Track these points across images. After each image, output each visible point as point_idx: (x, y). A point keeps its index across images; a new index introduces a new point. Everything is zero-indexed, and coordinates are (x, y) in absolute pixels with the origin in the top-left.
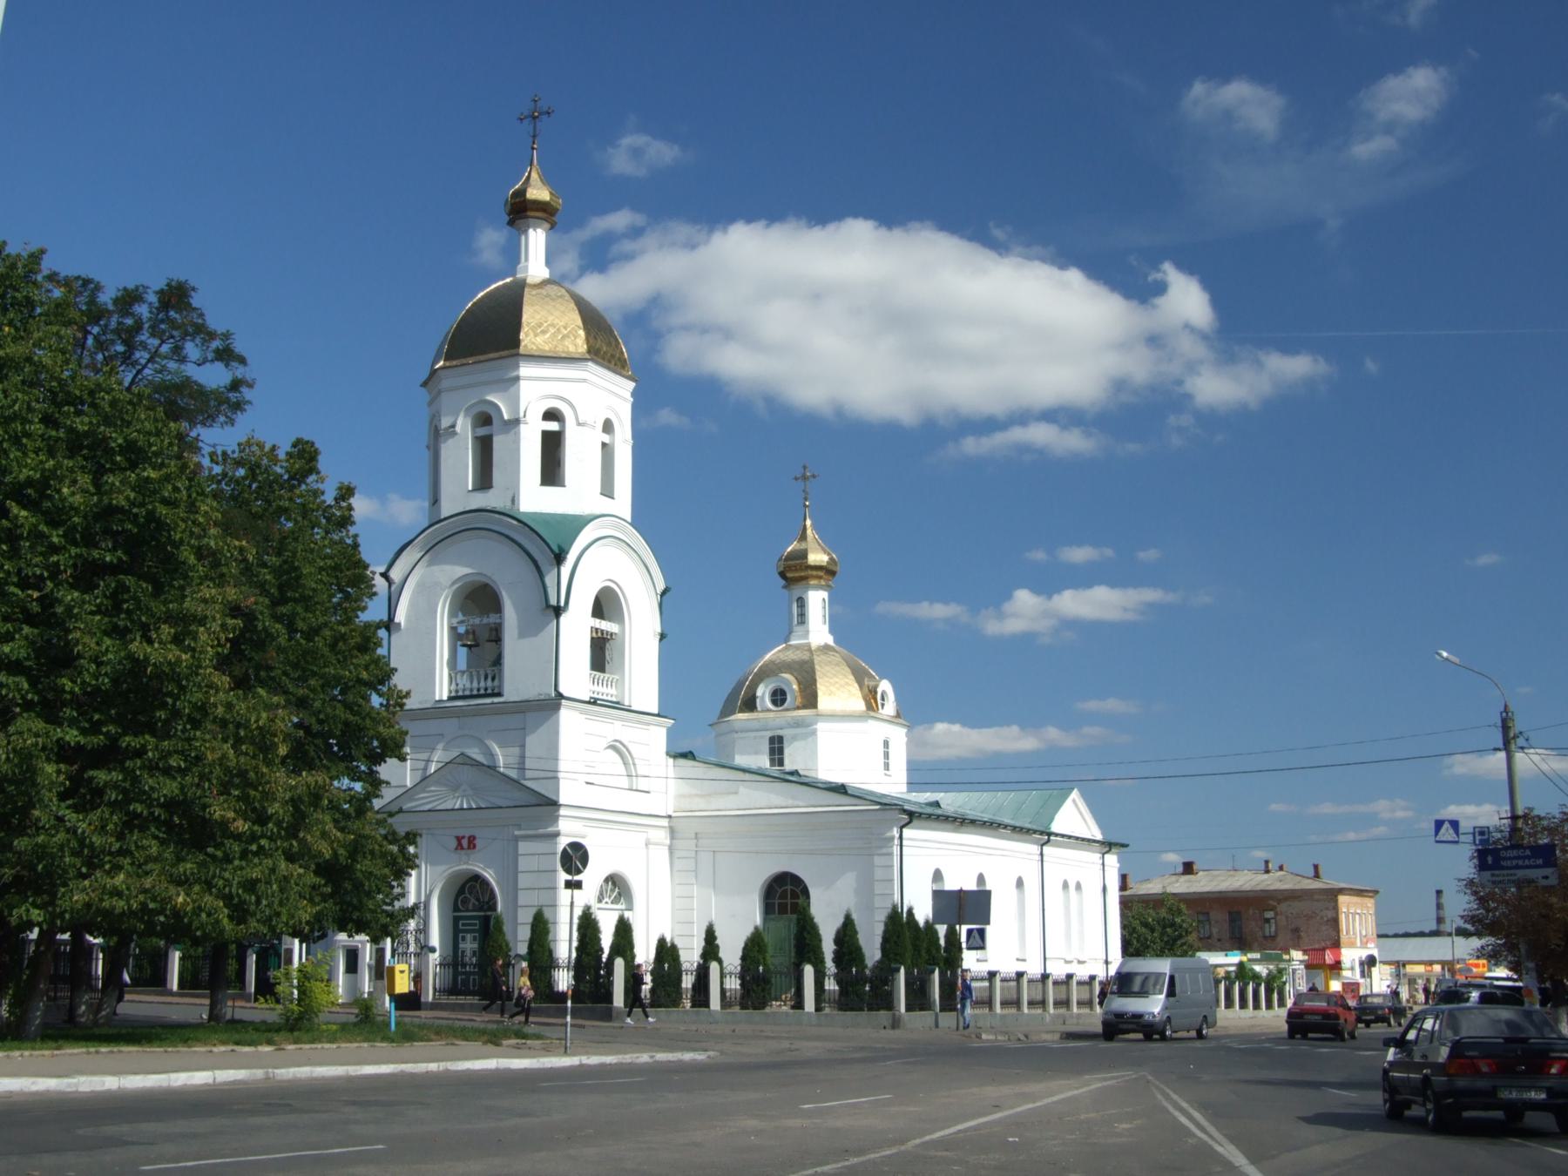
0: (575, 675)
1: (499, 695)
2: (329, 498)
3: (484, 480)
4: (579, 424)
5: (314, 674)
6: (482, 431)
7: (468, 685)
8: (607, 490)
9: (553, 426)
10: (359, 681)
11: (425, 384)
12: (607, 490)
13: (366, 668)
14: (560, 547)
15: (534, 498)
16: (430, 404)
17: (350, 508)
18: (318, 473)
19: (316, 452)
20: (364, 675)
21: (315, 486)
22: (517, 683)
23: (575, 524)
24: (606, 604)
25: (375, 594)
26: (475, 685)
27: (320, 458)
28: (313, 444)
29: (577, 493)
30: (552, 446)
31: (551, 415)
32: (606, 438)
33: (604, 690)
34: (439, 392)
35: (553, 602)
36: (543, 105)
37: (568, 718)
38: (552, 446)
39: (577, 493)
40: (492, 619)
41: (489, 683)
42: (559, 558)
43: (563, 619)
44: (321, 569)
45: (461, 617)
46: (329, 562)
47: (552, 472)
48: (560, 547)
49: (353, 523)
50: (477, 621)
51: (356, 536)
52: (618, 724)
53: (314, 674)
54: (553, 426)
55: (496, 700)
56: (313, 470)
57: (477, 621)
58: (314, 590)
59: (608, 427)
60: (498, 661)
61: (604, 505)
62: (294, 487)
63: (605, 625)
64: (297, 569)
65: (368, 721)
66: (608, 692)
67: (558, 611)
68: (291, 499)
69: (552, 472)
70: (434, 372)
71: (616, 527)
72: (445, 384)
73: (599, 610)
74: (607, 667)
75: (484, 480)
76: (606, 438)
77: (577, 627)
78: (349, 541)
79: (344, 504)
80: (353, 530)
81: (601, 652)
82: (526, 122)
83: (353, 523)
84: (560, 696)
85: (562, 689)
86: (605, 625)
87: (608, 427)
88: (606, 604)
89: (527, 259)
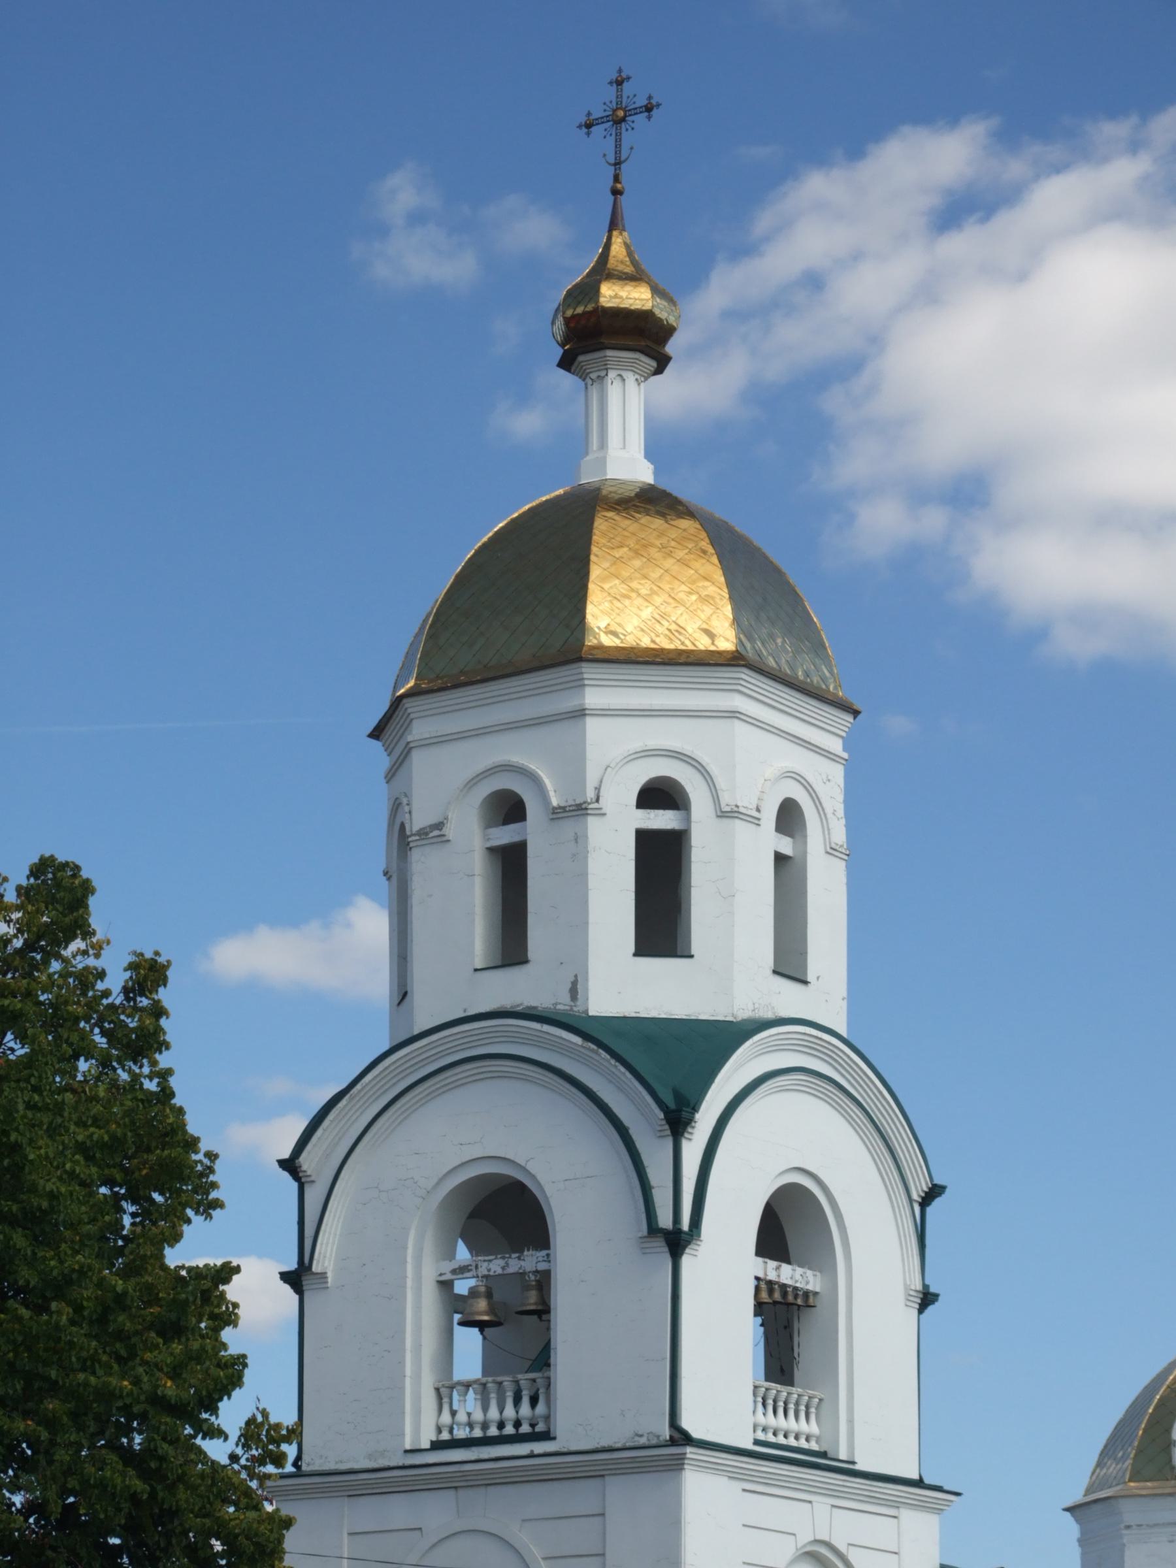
0: (721, 1385)
1: (546, 1436)
2: (115, 981)
3: (511, 946)
4: (722, 815)
5: (53, 1388)
6: (505, 835)
7: (478, 1416)
8: (790, 964)
9: (662, 820)
10: (158, 1401)
11: (377, 733)
12: (790, 964)
13: (175, 1373)
14: (678, 1096)
15: (625, 985)
16: (390, 776)
17: (158, 1011)
18: (87, 933)
19: (87, 888)
20: (169, 1387)
21: (80, 963)
22: (589, 1402)
23: (716, 1041)
24: (787, 1224)
25: (217, 1204)
26: (493, 1413)
27: (92, 901)
28: (77, 868)
29: (724, 970)
30: (662, 868)
31: (658, 794)
32: (786, 846)
33: (791, 1424)
34: (408, 751)
35: (665, 1220)
36: (635, 92)
37: (703, 1491)
38: (662, 868)
39: (724, 970)
40: (531, 1261)
41: (525, 1409)
42: (677, 1122)
43: (687, 1261)
44: (81, 1148)
45: (463, 1253)
46: (97, 1133)
47: (661, 925)
48: (678, 1096)
49: (164, 1045)
50: (496, 1266)
51: (169, 1072)
52: (822, 1504)
53: (53, 1388)
54: (662, 820)
55: (539, 1447)
56: (81, 928)
57: (496, 1266)
58: (53, 1196)
59: (789, 817)
60: (543, 1360)
61: (786, 999)
62: (35, 966)
63: (787, 1274)
64: (16, 1148)
65: (182, 1494)
66: (801, 1429)
67: (677, 1242)
68: (29, 994)
69: (661, 925)
70: (397, 703)
71: (811, 1048)
72: (419, 730)
73: (774, 1237)
74: (798, 1374)
75: (511, 946)
76: (786, 846)
77: (723, 1274)
78: (151, 1086)
79: (144, 1002)
80: (164, 1060)
81: (786, 1328)
82: (597, 130)
83: (164, 1045)
84: (681, 1438)
85: (688, 1422)
86: (787, 1274)
87: (789, 817)
88: (787, 1224)
89: (603, 445)
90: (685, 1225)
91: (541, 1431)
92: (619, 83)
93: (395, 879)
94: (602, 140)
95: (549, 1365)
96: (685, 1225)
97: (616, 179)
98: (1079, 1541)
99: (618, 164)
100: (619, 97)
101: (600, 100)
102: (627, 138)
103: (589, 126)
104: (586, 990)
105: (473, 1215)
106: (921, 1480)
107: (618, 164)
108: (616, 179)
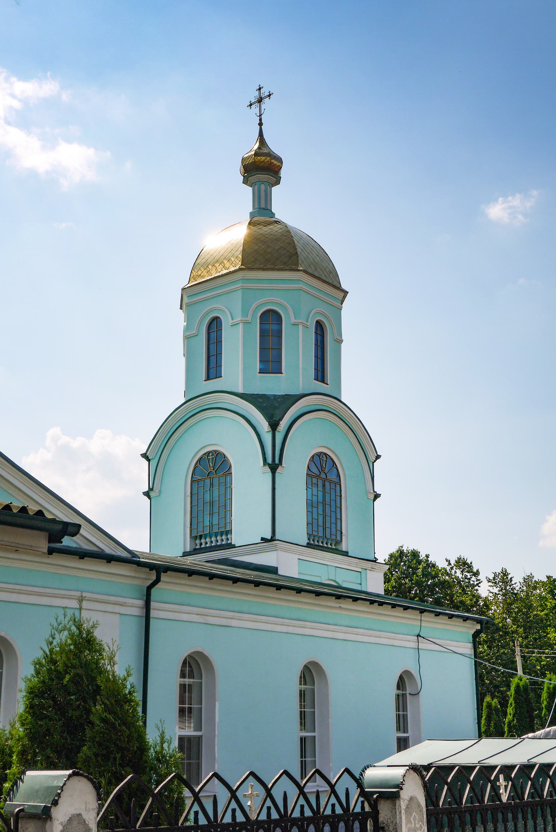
36: (265, 92)
90: (277, 461)
91: (290, 830)
92: (260, 89)
93: (154, 463)
94: (255, 109)
95: (244, 167)
96: (277, 461)
97: (260, 120)
98: (415, 554)
99: (260, 115)
100: (260, 94)
101: (253, 96)
102: (263, 107)
103: (251, 105)
104: (189, 354)
105: (289, 231)
106: (421, 613)
107: (260, 115)
108: (260, 120)
